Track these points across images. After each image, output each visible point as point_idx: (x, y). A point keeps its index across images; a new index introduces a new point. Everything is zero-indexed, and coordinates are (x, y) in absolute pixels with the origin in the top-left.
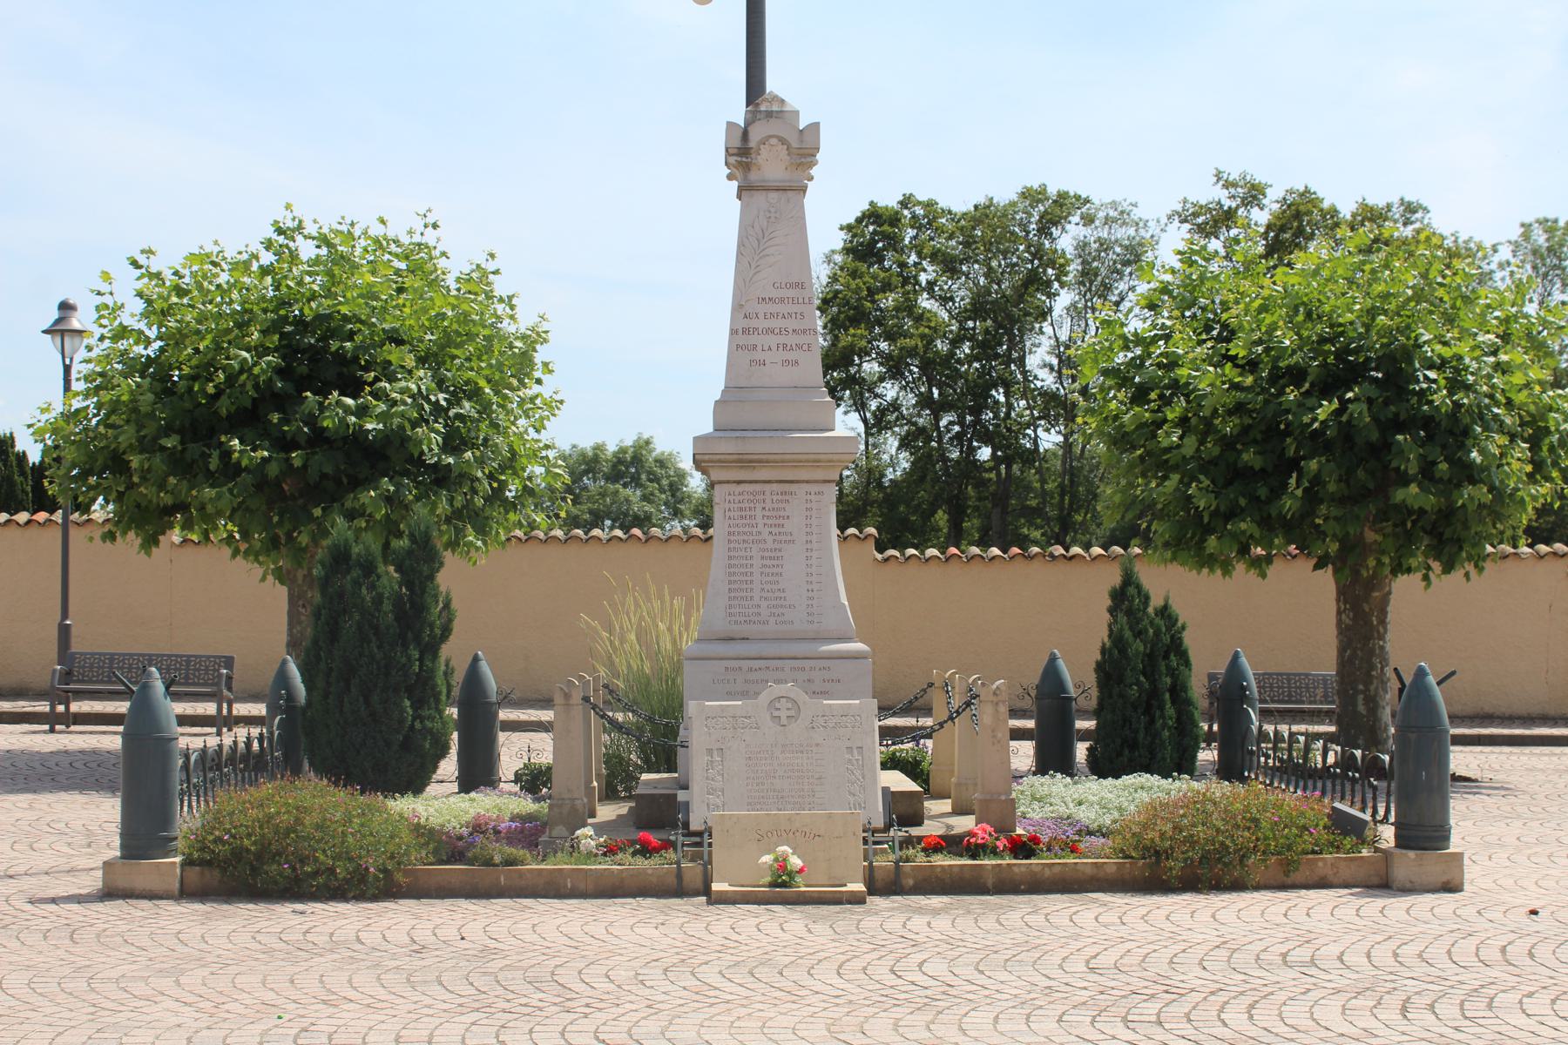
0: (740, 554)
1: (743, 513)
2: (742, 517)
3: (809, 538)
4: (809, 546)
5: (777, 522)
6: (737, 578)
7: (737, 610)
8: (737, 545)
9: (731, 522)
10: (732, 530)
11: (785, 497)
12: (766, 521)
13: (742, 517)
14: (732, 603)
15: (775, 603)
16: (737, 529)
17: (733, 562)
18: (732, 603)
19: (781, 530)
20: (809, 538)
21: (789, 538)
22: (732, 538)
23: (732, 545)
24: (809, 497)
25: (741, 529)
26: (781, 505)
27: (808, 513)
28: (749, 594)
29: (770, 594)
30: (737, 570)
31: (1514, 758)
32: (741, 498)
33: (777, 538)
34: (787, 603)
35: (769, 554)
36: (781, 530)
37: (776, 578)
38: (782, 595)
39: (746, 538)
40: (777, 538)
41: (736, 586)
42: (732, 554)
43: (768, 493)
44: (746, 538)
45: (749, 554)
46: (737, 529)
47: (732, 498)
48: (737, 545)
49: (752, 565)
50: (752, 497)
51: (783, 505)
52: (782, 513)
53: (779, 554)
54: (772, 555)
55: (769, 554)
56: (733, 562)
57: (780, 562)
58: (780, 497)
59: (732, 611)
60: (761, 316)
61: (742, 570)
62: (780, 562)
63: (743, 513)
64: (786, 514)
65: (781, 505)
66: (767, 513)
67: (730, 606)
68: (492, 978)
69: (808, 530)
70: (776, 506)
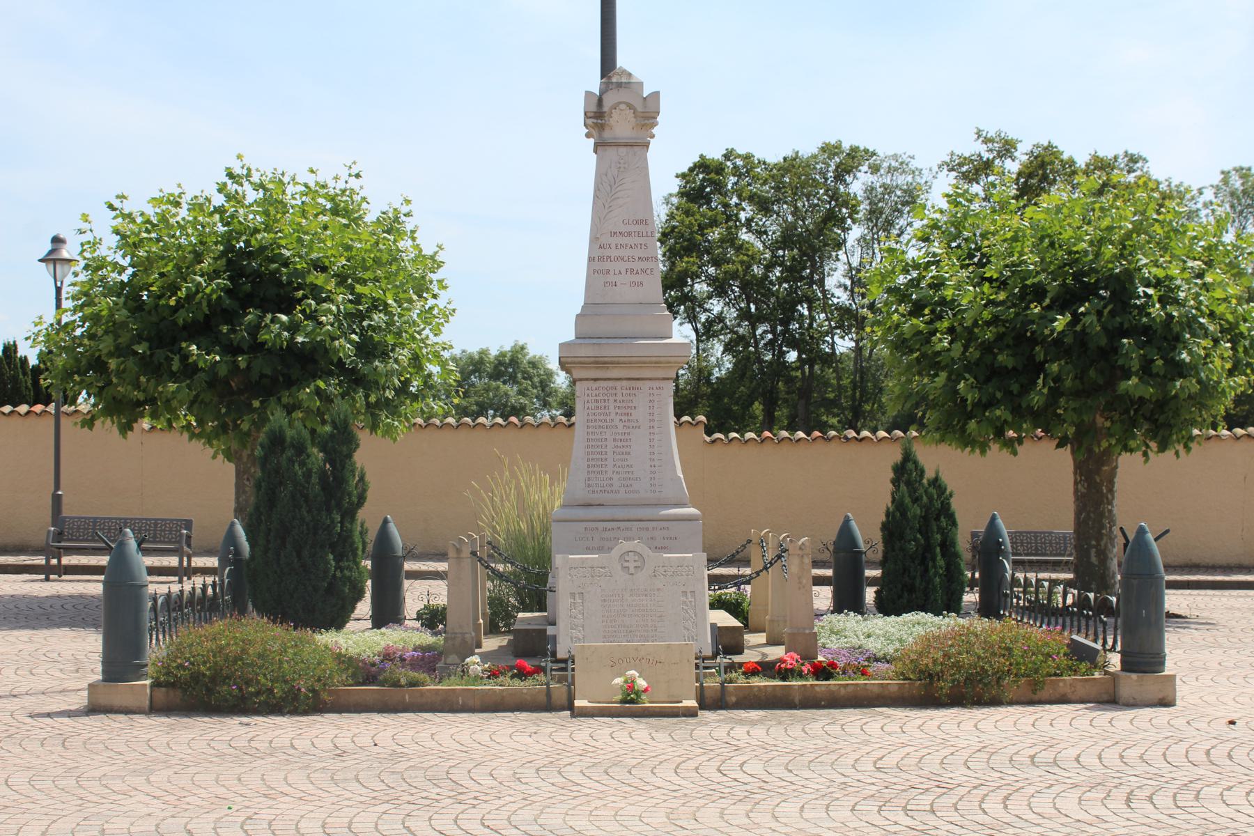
1: (599, 405)
2: (598, 407)
4: (652, 431)
5: (626, 411)
6: (594, 457)
8: (594, 430)
9: (590, 411)
10: (590, 418)
13: (598, 407)
15: (625, 476)
17: (590, 443)
19: (630, 418)
20: (652, 424)
21: (635, 424)
22: (590, 424)
24: (651, 391)
25: (598, 417)
27: (651, 404)
29: (620, 469)
33: (626, 424)
35: (620, 437)
36: (630, 418)
39: (601, 424)
40: (626, 424)
42: (590, 437)
43: (618, 388)
47: (590, 392)
48: (594, 430)
49: (606, 446)
52: (630, 404)
54: (623, 437)
56: (590, 443)
57: (628, 444)
58: (628, 392)
59: (591, 482)
61: (598, 450)
62: (628, 444)
63: (599, 405)
65: (628, 398)
69: (651, 411)
70: (624, 398)
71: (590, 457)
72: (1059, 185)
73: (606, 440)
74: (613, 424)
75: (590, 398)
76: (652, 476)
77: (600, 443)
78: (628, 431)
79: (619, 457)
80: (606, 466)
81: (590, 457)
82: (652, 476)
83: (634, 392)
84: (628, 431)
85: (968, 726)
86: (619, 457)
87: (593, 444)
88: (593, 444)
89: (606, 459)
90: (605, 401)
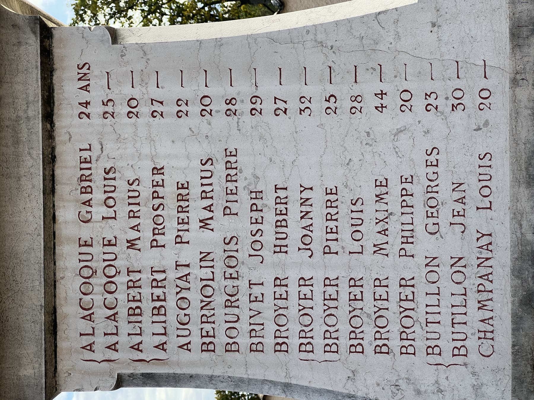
0: (268, 314)
1: (147, 305)
2: (157, 311)
3: (219, 106)
4: (246, 107)
5: (171, 203)
6: (344, 328)
7: (445, 329)
8: (244, 326)
9: (173, 342)
10: (196, 340)
11: (98, 182)
12: (169, 238)
13: (157, 311)
14: (420, 344)
15: (420, 212)
16: (195, 327)
17: (294, 342)
18: (420, 344)
19: (195, 190)
20: (219, 106)
21: (219, 169)
22: (221, 339)
23: (244, 341)
24: (96, 109)
25: (195, 312)
26: (121, 194)
27: (145, 109)
28: (394, 290)
29: (394, 227)
30: (319, 328)
31: (39, 278)
32: (101, 313)
33: (219, 204)
34: (422, 171)
35: (268, 228)
36: (195, 190)
37: (344, 209)
38: (395, 188)
39: (219, 299)
40: (219, 204)
41: (369, 331)
42: (269, 341)
43: (86, 232)
44: (219, 299)
45: (269, 290)
46: (195, 327)
47: (100, 341)
48: (244, 326)
49: (303, 282)
50: (99, 280)
51: (121, 185)
52: (146, 190)
53: (269, 199)
54: (270, 217)
55: (268, 228)
56: (294, 342)
57: (294, 195)
58: (98, 196)
59: (446, 345)
60: (84, 96)
61: (318, 312)
62: (294, 195)
63: (147, 305)
64: (147, 177)
65: (121, 194)
66: (147, 234)
67: (430, 350)
68: (232, 175)
69: (195, 109)
70: (123, 210)
71: (344, 342)
72: (194, 21)
73: (278, 282)
74: (218, 254)
75: (123, 339)
76: (418, 103)
77: (293, 301)
78: (244, 196)
79: (345, 233)
80: (378, 283)
81: (344, 342)
82: (418, 103)
83: (98, 175)
84: (244, 196)
85: (125, 215)
86: (345, 233)
87: (294, 328)
88: (294, 328)
89: (354, 283)
90: (133, 285)
